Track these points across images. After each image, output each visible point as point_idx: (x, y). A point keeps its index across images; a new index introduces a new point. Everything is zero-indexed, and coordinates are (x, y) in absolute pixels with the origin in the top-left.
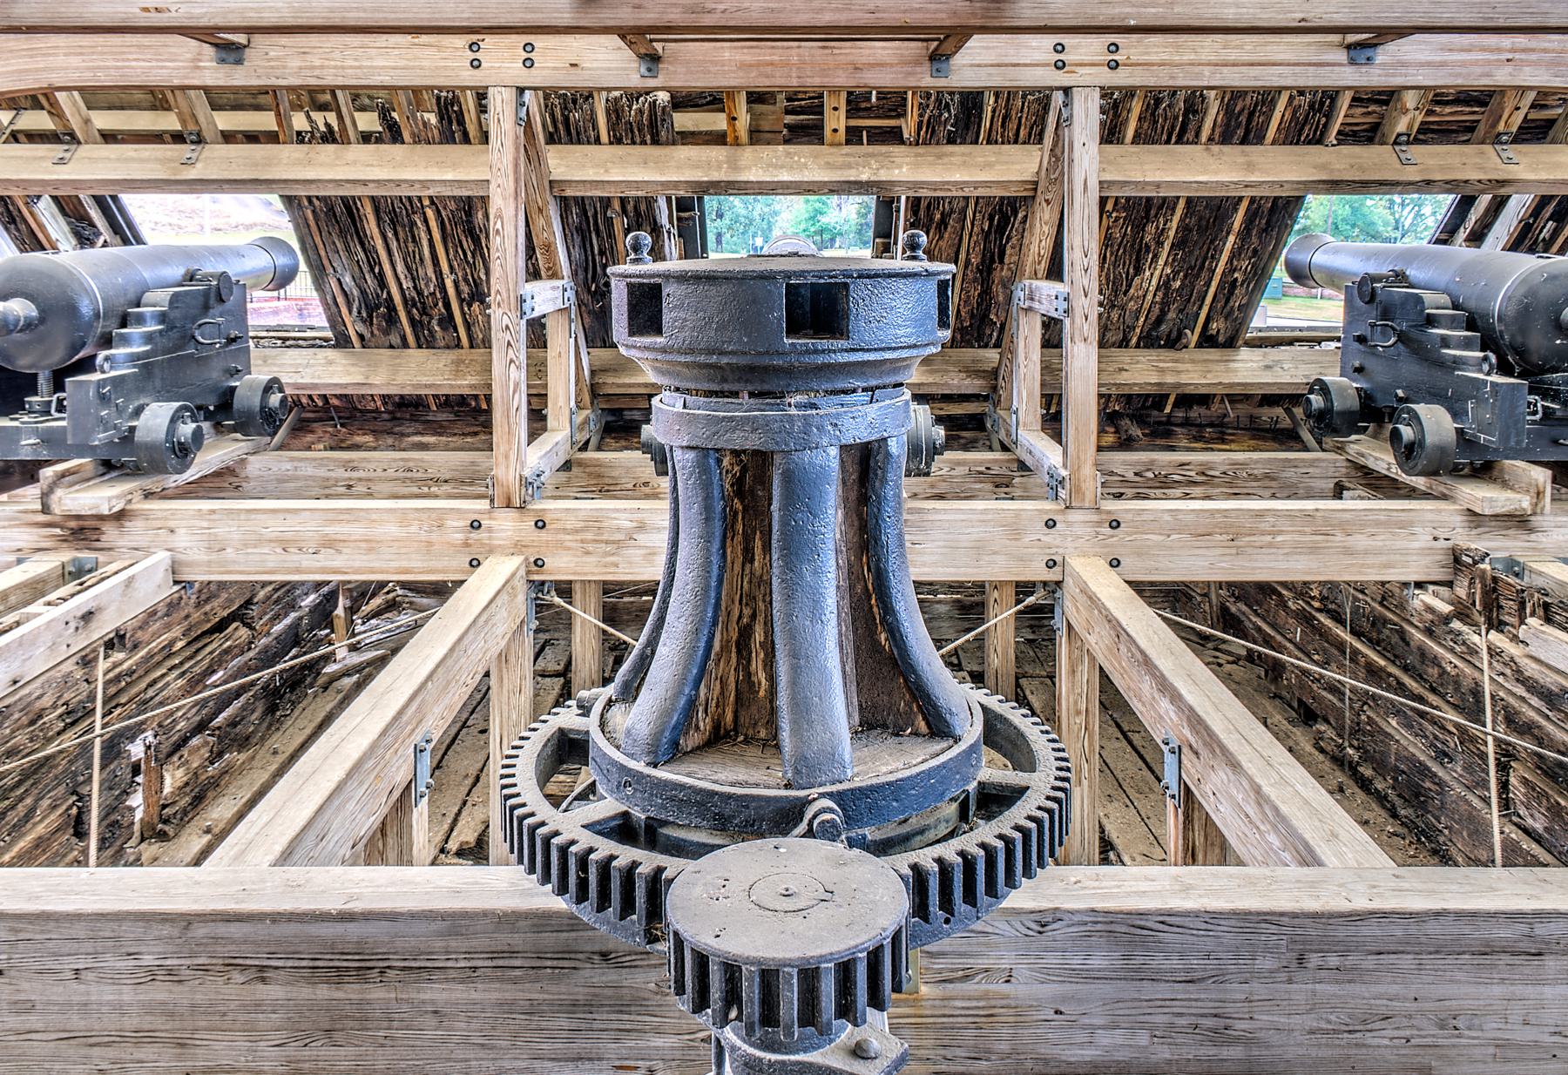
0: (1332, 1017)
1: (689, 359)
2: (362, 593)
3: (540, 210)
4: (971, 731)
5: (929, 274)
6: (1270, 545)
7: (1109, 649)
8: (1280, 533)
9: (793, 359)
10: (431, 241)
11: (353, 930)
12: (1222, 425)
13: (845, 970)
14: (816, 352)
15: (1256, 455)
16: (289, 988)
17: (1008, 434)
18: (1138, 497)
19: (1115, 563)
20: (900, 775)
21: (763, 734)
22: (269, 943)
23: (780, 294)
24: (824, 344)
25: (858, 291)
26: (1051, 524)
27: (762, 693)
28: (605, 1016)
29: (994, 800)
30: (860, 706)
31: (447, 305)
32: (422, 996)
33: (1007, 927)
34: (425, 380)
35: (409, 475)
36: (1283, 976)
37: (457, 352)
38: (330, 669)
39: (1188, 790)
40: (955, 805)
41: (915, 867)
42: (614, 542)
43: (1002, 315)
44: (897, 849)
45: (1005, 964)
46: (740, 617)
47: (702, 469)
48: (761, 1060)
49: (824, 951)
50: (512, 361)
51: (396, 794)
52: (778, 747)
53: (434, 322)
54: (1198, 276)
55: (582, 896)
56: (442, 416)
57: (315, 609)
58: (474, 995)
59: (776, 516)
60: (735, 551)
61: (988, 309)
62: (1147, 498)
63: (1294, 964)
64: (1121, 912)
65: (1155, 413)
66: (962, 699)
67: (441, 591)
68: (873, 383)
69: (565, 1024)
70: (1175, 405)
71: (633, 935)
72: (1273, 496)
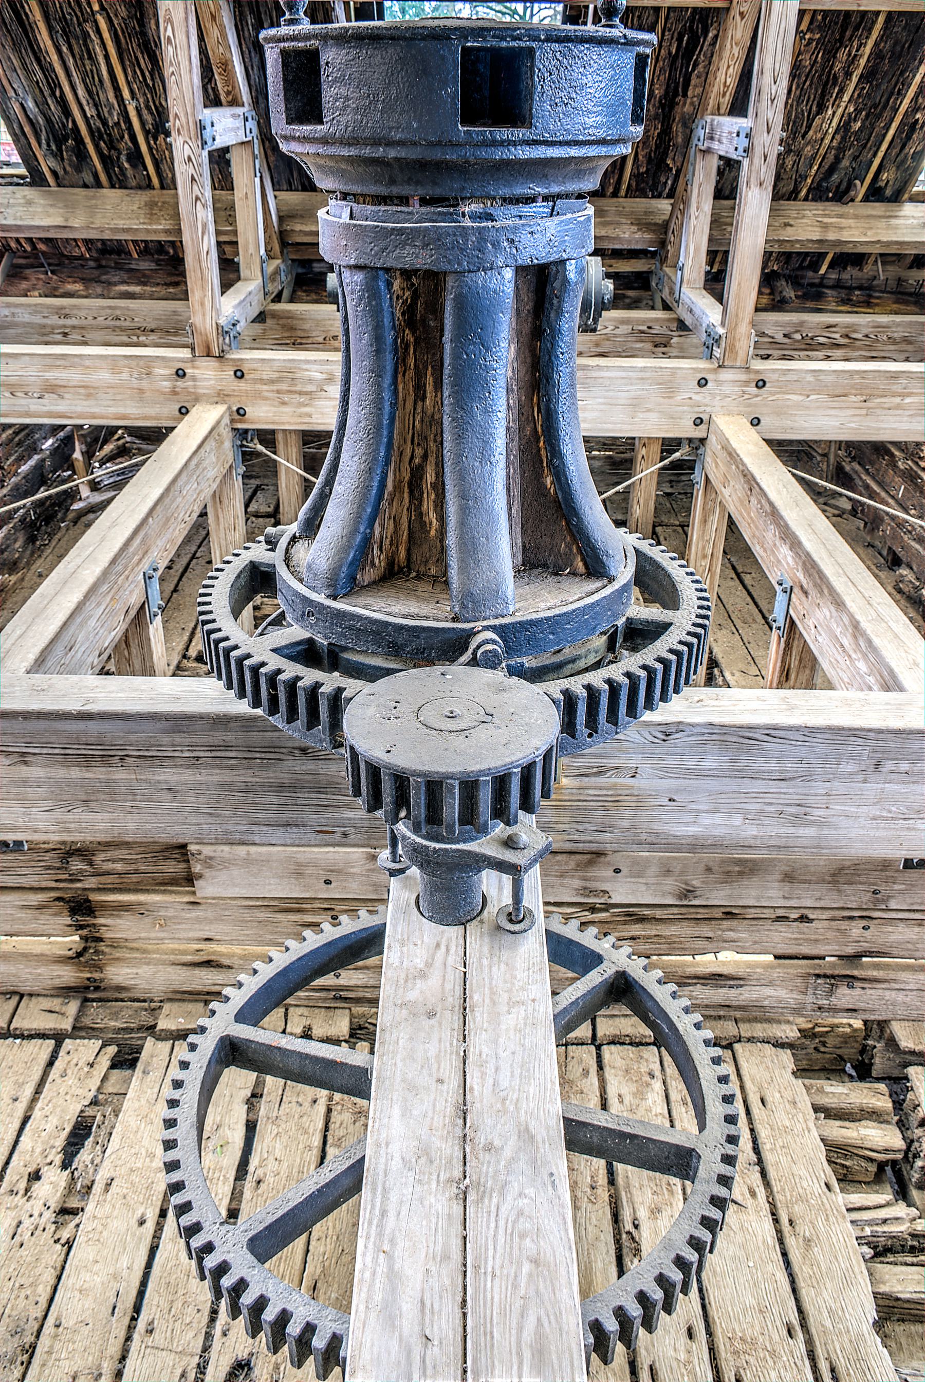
0: (893, 809)
1: (353, 152)
2: (97, 436)
3: (214, 18)
4: (624, 573)
5: (630, 43)
6: (898, 407)
7: (741, 501)
8: (910, 395)
9: (468, 153)
10: (107, 57)
11: (93, 727)
12: (870, 288)
13: (501, 782)
14: (495, 143)
15: (898, 318)
16: (48, 770)
17: (672, 293)
18: (783, 358)
19: (756, 422)
20: (557, 611)
21: (433, 571)
22: (24, 735)
23: (455, 61)
24: (503, 133)
25: (546, 59)
26: (702, 383)
27: (433, 533)
28: (306, 795)
29: (638, 635)
30: (524, 546)
31: (133, 138)
32: (157, 777)
33: (638, 736)
34: (122, 224)
35: (118, 323)
36: (861, 777)
37: (150, 193)
38: (76, 506)
39: (792, 622)
40: (604, 638)
41: (566, 693)
42: (306, 393)
43: (679, 159)
44: (551, 676)
45: (632, 764)
46: (412, 458)
47: (371, 293)
48: (427, 847)
49: (484, 766)
50: (197, 198)
51: (133, 613)
52: (446, 583)
53: (123, 158)
54: (879, 116)
55: (273, 709)
56: (145, 265)
57: (55, 451)
58: (199, 778)
59: (448, 348)
60: (406, 388)
61: (665, 154)
62: (791, 358)
63: (872, 768)
64: (734, 726)
65: (810, 274)
66: (621, 545)
67: (154, 436)
68: (555, 189)
69: (275, 800)
70: (831, 266)
71: (321, 741)
72: (907, 360)
